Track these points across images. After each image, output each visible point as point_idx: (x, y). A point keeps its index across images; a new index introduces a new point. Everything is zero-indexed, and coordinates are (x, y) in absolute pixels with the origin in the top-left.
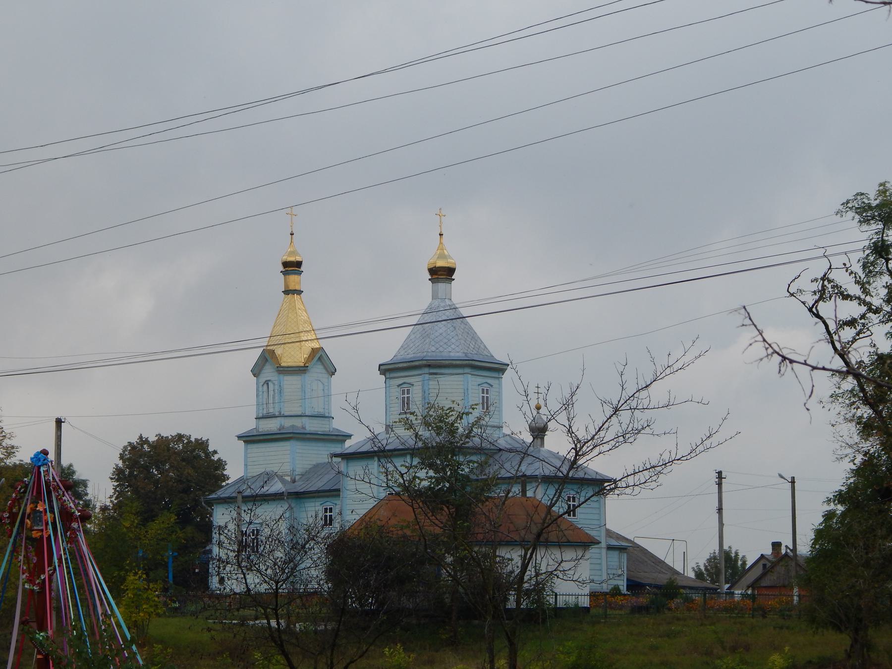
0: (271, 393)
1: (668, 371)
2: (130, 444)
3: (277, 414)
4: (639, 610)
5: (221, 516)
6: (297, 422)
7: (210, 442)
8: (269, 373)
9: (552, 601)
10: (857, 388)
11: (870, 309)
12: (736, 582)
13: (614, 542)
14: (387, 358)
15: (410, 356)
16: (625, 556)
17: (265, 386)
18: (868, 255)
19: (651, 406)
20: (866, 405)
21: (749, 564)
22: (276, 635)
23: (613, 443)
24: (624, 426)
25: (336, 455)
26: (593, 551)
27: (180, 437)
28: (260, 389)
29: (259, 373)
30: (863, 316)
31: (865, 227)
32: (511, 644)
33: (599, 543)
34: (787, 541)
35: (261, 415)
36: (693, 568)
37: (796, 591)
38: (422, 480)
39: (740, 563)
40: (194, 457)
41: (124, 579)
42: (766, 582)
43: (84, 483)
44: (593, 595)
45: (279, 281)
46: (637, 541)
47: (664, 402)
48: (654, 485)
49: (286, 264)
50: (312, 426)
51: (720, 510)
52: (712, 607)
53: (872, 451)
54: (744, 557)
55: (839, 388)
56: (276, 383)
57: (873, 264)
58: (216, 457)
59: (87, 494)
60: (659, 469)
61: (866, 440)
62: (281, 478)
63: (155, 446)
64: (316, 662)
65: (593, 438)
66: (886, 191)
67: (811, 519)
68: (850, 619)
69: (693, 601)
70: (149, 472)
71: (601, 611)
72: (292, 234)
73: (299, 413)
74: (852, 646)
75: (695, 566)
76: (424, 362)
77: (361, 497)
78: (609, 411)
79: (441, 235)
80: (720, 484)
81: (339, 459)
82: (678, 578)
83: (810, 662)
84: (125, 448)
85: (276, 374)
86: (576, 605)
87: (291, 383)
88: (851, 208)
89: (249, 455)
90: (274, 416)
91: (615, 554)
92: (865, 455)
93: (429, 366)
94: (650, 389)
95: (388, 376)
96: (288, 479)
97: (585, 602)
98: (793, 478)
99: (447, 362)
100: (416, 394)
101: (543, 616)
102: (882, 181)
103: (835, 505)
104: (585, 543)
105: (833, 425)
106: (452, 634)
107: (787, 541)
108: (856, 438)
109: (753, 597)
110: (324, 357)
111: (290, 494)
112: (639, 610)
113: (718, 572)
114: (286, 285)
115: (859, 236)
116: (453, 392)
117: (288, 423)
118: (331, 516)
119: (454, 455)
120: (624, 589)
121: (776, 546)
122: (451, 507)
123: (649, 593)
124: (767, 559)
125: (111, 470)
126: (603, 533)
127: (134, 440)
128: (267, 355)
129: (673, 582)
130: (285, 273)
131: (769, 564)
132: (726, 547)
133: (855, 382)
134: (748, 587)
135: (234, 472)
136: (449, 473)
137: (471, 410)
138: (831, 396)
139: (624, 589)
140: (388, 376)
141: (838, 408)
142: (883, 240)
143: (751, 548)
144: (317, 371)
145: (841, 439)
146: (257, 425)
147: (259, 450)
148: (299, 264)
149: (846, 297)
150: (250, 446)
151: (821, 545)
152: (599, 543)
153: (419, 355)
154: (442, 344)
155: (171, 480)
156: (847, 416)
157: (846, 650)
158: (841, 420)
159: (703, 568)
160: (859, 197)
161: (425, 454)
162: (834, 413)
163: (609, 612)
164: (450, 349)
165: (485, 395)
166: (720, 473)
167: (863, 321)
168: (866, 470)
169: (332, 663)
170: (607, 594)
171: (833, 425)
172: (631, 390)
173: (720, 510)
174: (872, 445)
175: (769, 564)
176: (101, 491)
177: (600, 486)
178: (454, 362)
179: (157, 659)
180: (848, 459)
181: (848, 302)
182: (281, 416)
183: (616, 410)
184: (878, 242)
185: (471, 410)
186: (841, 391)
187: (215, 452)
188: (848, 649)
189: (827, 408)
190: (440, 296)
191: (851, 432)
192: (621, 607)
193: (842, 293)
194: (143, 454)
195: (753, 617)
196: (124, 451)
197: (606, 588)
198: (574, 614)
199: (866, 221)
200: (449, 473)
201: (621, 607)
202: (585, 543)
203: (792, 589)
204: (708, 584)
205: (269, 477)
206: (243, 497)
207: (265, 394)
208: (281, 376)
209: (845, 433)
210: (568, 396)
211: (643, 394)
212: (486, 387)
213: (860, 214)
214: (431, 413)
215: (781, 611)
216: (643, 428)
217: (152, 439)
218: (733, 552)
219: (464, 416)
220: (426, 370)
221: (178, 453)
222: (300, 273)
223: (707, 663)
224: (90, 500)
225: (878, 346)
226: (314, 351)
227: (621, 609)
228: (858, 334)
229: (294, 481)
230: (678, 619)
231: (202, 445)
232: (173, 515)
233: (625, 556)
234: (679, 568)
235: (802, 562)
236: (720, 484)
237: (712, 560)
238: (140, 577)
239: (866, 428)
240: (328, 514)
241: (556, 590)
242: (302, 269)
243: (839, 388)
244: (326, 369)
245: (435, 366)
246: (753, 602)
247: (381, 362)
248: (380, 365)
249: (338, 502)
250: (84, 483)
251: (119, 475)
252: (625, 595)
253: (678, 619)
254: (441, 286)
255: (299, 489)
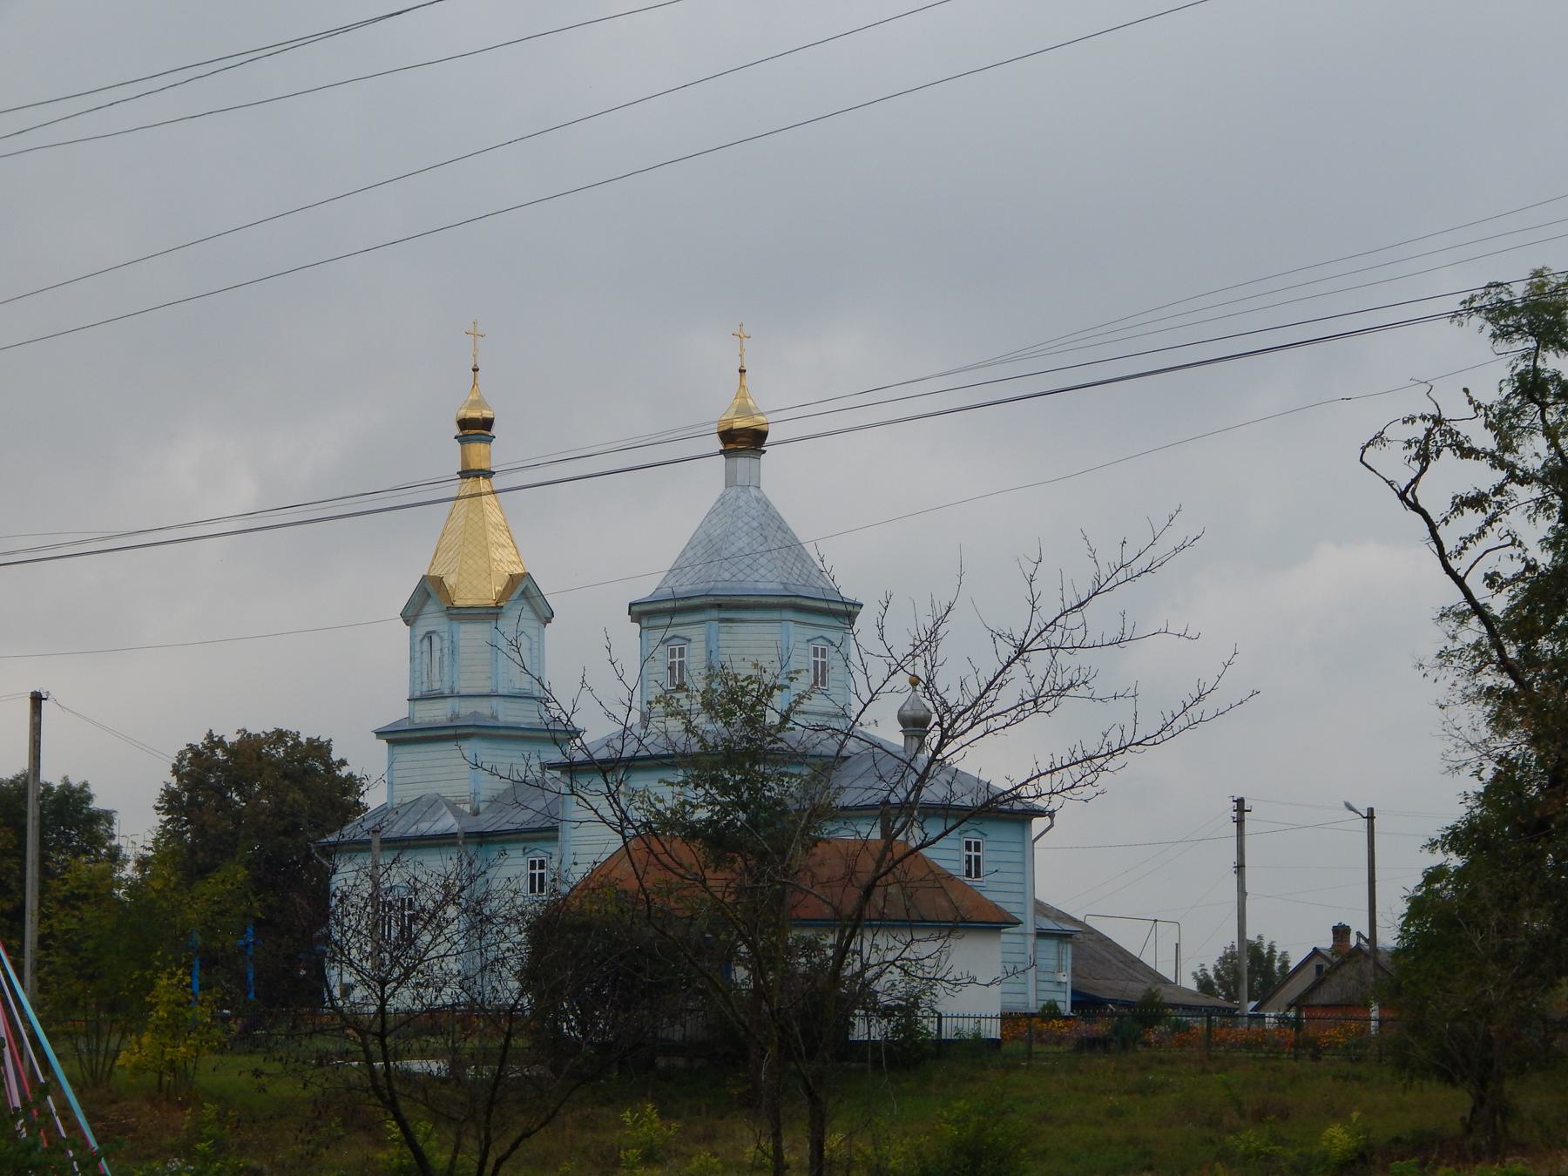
0: (437, 654)
1: (1121, 576)
2: (191, 747)
3: (447, 692)
4: (1091, 1044)
5: (347, 876)
6: (484, 708)
7: (334, 746)
8: (432, 619)
9: (932, 1027)
10: (1486, 641)
11: (1512, 477)
12: (1269, 998)
13: (1049, 925)
14: (644, 590)
15: (685, 586)
16: (1068, 950)
17: (426, 642)
18: (1508, 397)
19: (1088, 643)
20: (1502, 671)
21: (1293, 965)
22: (382, 1082)
23: (1014, 713)
24: (1037, 683)
25: (552, 766)
26: (1008, 937)
27: (280, 735)
28: (417, 647)
29: (417, 616)
30: (1499, 490)
31: (1502, 345)
32: (814, 1100)
33: (1017, 923)
34: (1359, 925)
35: (417, 694)
36: (1194, 974)
37: (1374, 1013)
38: (695, 807)
39: (1277, 964)
40: (305, 771)
41: (150, 986)
42: (1322, 997)
43: (108, 817)
44: (1007, 1018)
45: (450, 456)
46: (1091, 922)
47: (1113, 634)
48: (1089, 791)
49: (464, 424)
50: (511, 713)
51: (1240, 867)
52: (1223, 1041)
53: (1513, 754)
54: (1284, 954)
55: (1454, 638)
56: (446, 636)
57: (1517, 413)
58: (344, 772)
59: (112, 837)
60: (1098, 762)
61: (1503, 734)
62: (453, 807)
63: (233, 751)
64: (459, 1135)
65: (974, 705)
66: (1544, 285)
67: (1403, 875)
68: (1471, 1060)
69: (1188, 1029)
70: (224, 797)
71: (1022, 1046)
72: (475, 370)
73: (486, 691)
74: (1474, 1110)
75: (1197, 970)
76: (711, 600)
77: (589, 843)
78: (1007, 651)
79: (742, 371)
80: (1240, 822)
81: (557, 774)
82: (1164, 989)
83: (1397, 1140)
84: (182, 755)
85: (445, 619)
86: (977, 1036)
87: (473, 635)
88: (1478, 310)
89: (395, 766)
90: (442, 697)
91: (1049, 948)
92: (1498, 763)
93: (719, 606)
94: (1087, 609)
95: (645, 624)
96: (467, 808)
97: (993, 1030)
98: (1371, 810)
99: (752, 600)
100: (695, 660)
101: (917, 1055)
102: (1538, 267)
103: (1445, 853)
104: (994, 923)
105: (1442, 707)
106: (749, 1086)
107: (1359, 925)
108: (1485, 732)
109: (1297, 1024)
110: (533, 590)
111: (468, 835)
112: (1091, 1044)
113: (1237, 982)
114: (465, 460)
115: (1487, 366)
116: (752, 648)
117: (465, 708)
118: (541, 875)
119: (755, 762)
120: (1065, 1008)
121: (1341, 932)
122: (749, 856)
123: (1111, 1014)
124: (1324, 957)
125: (158, 793)
126: (1030, 909)
127: (199, 740)
128: (430, 588)
129: (1154, 995)
130: (463, 440)
131: (1327, 966)
132: (1251, 936)
133: (1484, 629)
134: (1290, 1006)
135: (374, 798)
136: (746, 795)
137: (787, 682)
138: (1440, 656)
139: (1065, 1008)
140: (645, 624)
141: (1451, 679)
142: (1536, 370)
143: (1296, 936)
144: (516, 619)
145: (1456, 733)
146: (412, 713)
147: (415, 757)
148: (487, 424)
149: (1468, 453)
150: (399, 750)
151: (1417, 926)
152: (1017, 923)
153: (702, 587)
154: (742, 566)
155: (263, 811)
156: (1469, 692)
157: (1463, 1119)
158: (1457, 698)
159: (1211, 973)
160: (1493, 290)
161: (700, 764)
162: (1444, 685)
163: (1036, 1047)
164: (757, 577)
165: (819, 659)
166: (1240, 802)
167: (1498, 498)
168: (1503, 787)
169: (488, 1137)
170: (1034, 1015)
171: (1442, 707)
172: (1049, 611)
173: (1240, 867)
174: (1513, 744)
175: (1327, 966)
176: (137, 828)
177: (1008, 813)
178: (764, 600)
179: (206, 1131)
180: (1468, 771)
181: (1470, 462)
182: (454, 695)
183: (1021, 650)
184: (1528, 372)
185: (787, 682)
186: (1458, 645)
187: (343, 763)
188: (1468, 1116)
189: (1431, 677)
190: (739, 481)
191: (1475, 718)
192: (1060, 1041)
193: (1459, 446)
194: (213, 766)
195: (1296, 1058)
196: (180, 761)
197: (1033, 1006)
198: (974, 1051)
199: (1505, 334)
200: (746, 795)
201: (1060, 1041)
202: (994, 923)
203: (1367, 1007)
204: (1221, 1000)
205: (432, 804)
206: (383, 841)
207: (426, 656)
208: (455, 623)
209: (1464, 722)
210: (929, 625)
211: (1074, 619)
212: (821, 644)
213: (1494, 321)
214: (714, 686)
215: (1347, 1047)
216: (1072, 685)
217: (231, 738)
218: (1266, 944)
219: (776, 692)
220: (714, 614)
221: (276, 765)
222: (490, 440)
223: (1212, 1142)
224: (118, 847)
225: (1526, 545)
226: (514, 580)
227: (1058, 1044)
228: (1489, 522)
229: (476, 813)
230: (1161, 1061)
231: (320, 749)
232: (241, 869)
233: (1068, 950)
234: (1167, 971)
235: (1382, 958)
236: (1240, 822)
237: (1228, 960)
238: (180, 981)
239: (1506, 709)
240: (537, 871)
241: (939, 1008)
242: (494, 432)
243: (1454, 638)
244: (535, 611)
245: (729, 607)
246: (1299, 1030)
247: (632, 600)
248: (631, 605)
249: (555, 851)
250: (108, 817)
251: (171, 802)
252: (1067, 1018)
253: (1161, 1061)
254: (742, 463)
255: (484, 827)
